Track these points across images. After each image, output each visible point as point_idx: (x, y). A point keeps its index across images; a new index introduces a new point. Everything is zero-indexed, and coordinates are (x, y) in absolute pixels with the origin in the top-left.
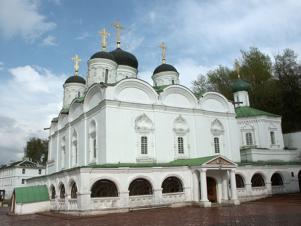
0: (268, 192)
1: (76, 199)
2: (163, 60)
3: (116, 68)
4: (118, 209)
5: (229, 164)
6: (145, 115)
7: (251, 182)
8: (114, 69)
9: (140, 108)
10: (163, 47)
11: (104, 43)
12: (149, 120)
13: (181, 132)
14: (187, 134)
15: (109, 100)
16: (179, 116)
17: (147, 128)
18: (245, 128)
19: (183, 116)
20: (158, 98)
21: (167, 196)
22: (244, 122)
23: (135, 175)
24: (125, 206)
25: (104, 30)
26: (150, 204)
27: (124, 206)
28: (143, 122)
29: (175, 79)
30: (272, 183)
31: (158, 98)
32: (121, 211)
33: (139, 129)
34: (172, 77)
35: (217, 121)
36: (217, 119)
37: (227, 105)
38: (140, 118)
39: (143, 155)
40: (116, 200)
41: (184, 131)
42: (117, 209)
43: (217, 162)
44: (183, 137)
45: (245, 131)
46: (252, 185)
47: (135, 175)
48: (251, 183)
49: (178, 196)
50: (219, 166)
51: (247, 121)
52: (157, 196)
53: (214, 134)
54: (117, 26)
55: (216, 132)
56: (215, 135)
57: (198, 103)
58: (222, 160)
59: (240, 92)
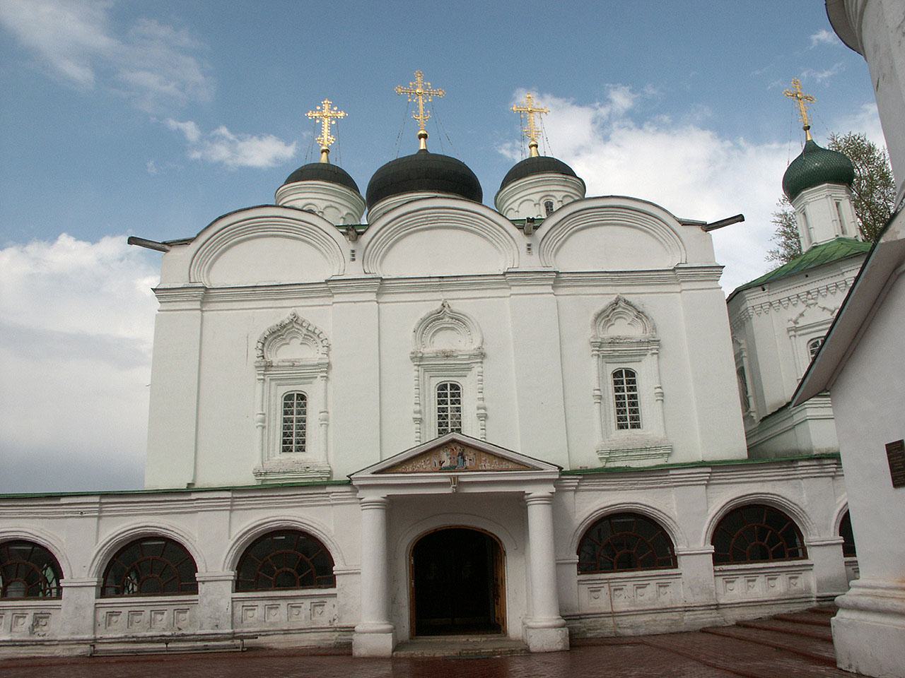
0: (819, 588)
1: (854, 559)
2: (530, 147)
3: (359, 212)
4: (52, 643)
5: (510, 466)
6: (295, 320)
7: (840, 535)
8: (354, 215)
9: (284, 299)
10: (529, 109)
11: (326, 141)
12: (312, 335)
13: (448, 362)
14: (477, 369)
15: (171, 287)
16: (438, 306)
17: (301, 363)
18: (802, 322)
19: (457, 306)
20: (353, 255)
21: (256, 603)
22: (798, 297)
23: (129, 523)
24: (78, 634)
25: (327, 107)
26: (180, 629)
27: (73, 633)
28: (296, 342)
29: (557, 197)
30: (843, 544)
31: (350, 257)
32: (60, 651)
33: (270, 369)
34: (543, 194)
35: (622, 304)
36: (623, 296)
37: (679, 237)
38: (278, 334)
39: (287, 455)
40: (46, 611)
41: (459, 360)
42: (48, 643)
43: (441, 463)
44: (461, 382)
45: (803, 334)
46: (713, 554)
47: (129, 523)
48: (712, 549)
49: (283, 604)
50: (448, 480)
51: (808, 293)
52: (210, 603)
53: (607, 358)
54: (418, 91)
55: (616, 347)
56: (615, 360)
57: (529, 249)
58: (470, 455)
59: (808, 193)
